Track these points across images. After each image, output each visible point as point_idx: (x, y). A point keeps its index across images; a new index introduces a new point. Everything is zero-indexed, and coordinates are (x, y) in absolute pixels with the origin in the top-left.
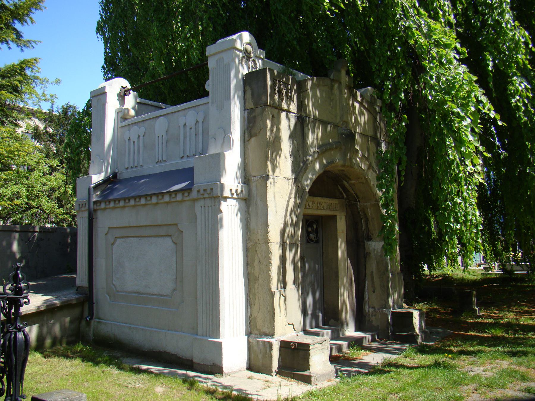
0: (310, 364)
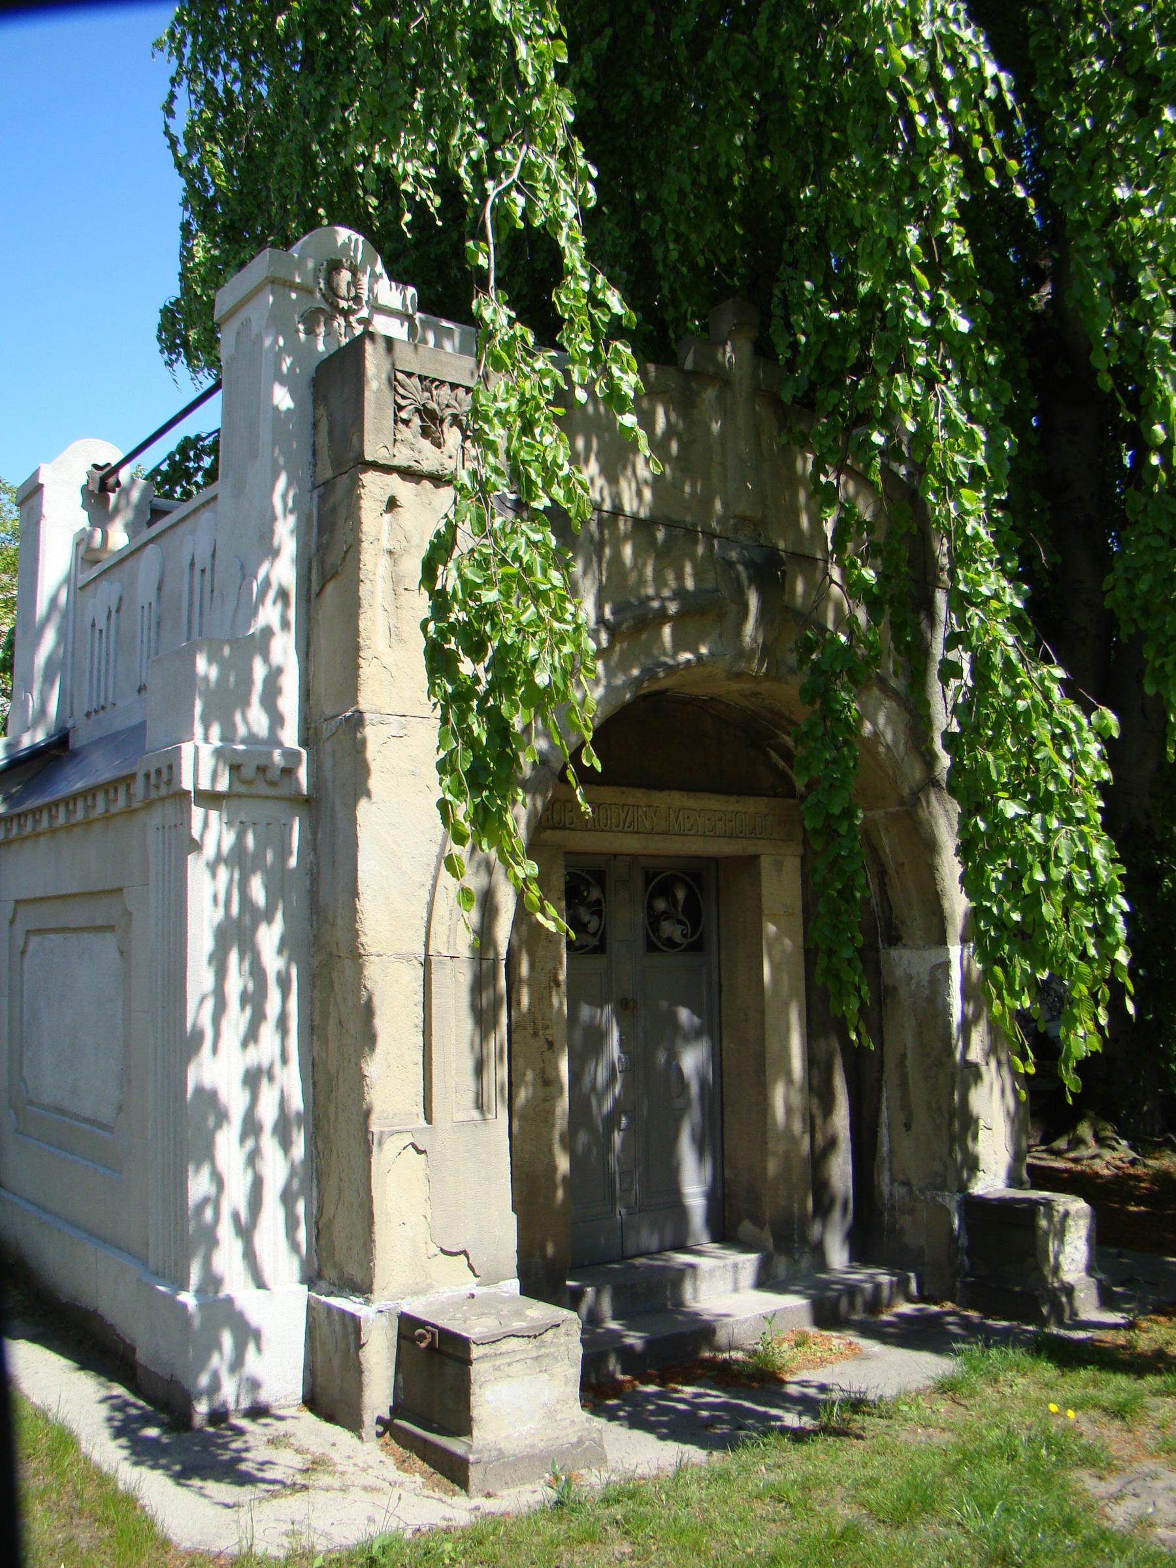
0: (475, 1413)
